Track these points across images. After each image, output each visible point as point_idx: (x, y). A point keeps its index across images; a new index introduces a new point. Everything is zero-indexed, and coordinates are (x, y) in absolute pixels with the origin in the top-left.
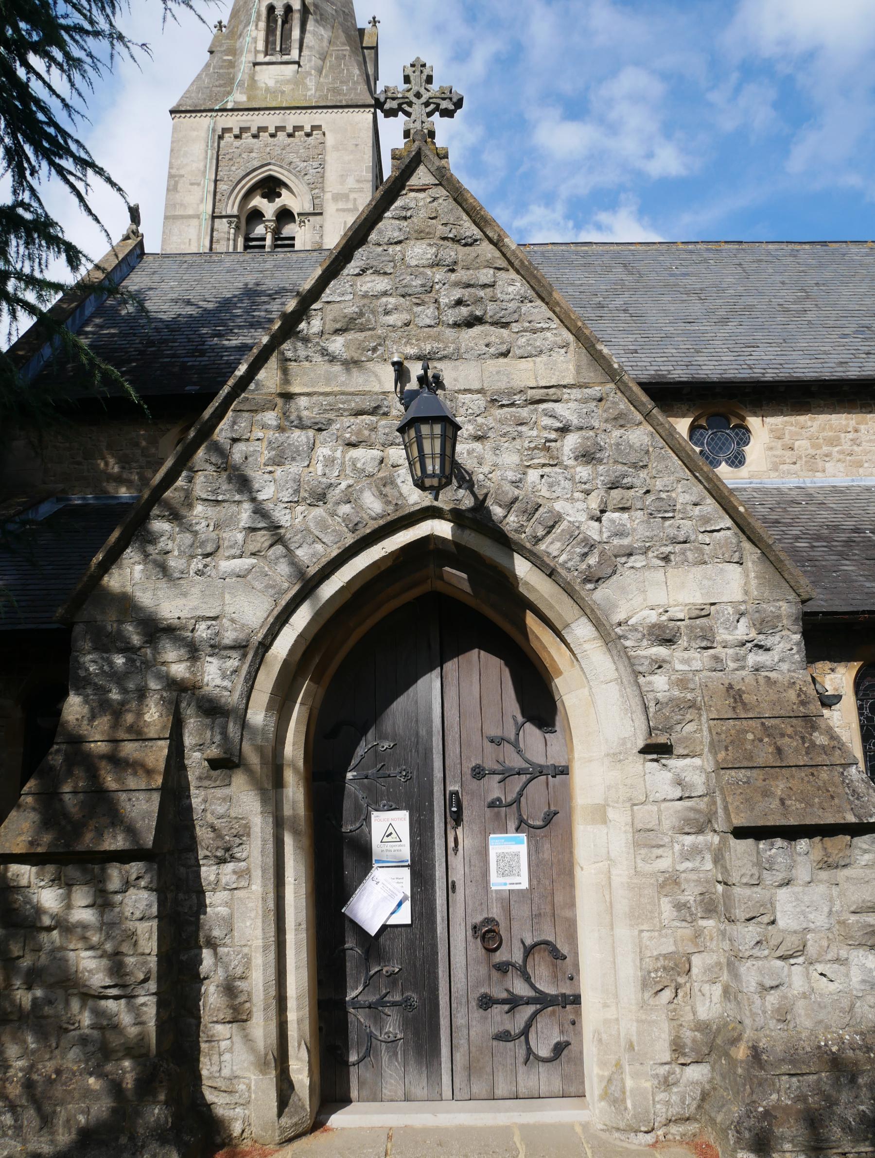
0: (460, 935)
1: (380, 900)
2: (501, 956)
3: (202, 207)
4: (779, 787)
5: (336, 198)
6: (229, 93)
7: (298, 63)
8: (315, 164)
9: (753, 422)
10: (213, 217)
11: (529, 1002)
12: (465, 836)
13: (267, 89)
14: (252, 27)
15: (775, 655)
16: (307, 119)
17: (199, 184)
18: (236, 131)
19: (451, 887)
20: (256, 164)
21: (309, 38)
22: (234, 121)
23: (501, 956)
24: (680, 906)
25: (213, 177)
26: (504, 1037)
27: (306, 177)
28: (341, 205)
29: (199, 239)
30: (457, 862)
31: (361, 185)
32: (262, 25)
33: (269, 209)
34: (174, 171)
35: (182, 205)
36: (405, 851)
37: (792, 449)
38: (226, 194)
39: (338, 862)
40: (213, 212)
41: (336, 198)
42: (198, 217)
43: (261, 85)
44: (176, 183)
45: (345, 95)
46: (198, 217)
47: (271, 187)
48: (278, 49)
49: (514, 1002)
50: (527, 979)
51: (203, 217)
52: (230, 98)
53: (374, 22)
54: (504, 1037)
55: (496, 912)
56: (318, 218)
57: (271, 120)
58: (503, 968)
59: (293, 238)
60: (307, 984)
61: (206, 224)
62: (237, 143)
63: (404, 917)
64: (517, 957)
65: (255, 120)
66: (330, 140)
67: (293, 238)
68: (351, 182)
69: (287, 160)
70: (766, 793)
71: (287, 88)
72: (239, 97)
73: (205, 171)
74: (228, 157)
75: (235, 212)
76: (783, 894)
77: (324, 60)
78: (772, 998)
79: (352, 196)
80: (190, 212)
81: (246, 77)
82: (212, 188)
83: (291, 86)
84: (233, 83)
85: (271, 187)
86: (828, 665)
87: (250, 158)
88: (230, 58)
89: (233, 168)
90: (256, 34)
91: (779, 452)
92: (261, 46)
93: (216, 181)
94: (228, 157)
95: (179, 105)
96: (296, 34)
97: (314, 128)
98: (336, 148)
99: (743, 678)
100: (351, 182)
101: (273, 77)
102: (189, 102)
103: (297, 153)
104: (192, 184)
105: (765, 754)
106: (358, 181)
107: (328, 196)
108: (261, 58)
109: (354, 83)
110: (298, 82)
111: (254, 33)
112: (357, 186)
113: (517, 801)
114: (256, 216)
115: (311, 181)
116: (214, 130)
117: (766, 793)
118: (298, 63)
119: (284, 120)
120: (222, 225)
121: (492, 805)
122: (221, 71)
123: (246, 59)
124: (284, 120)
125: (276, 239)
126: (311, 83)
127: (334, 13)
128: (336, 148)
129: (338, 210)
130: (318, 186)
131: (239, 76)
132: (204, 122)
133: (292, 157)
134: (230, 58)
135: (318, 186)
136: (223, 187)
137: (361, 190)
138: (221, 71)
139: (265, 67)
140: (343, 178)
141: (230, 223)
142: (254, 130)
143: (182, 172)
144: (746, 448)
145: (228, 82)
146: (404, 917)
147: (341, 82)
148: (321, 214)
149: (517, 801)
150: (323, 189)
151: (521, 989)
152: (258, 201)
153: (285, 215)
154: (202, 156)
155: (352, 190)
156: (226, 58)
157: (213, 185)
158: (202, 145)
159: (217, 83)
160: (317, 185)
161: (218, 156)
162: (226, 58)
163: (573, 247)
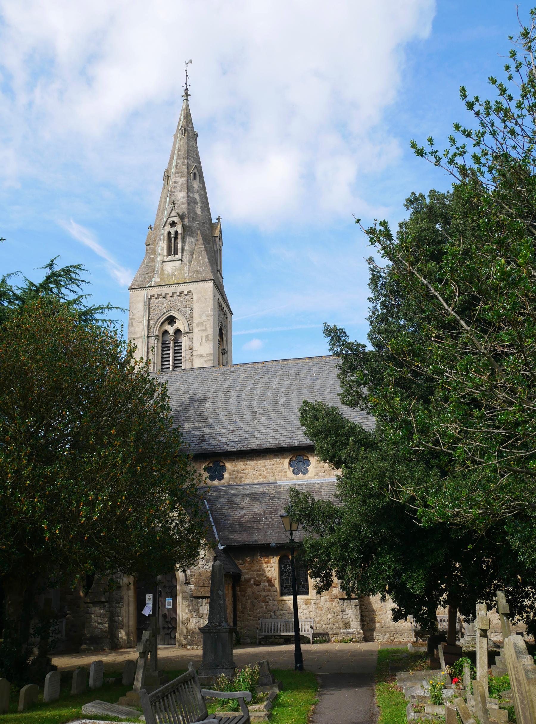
0: (160, 616)
1: (147, 611)
2: (167, 620)
3: (143, 333)
4: (202, 590)
5: (199, 324)
6: (153, 277)
7: (181, 260)
8: (189, 309)
9: (311, 459)
10: (148, 337)
11: (171, 628)
12: (161, 599)
13: (169, 274)
14: (161, 242)
15: (209, 566)
16: (184, 288)
17: (141, 322)
18: (156, 296)
19: (159, 608)
20: (165, 310)
21: (187, 247)
22: (154, 292)
23: (167, 620)
24: (189, 610)
25: (147, 319)
26: (166, 634)
27: (186, 315)
28: (200, 328)
29: (142, 348)
30: (160, 604)
31: (208, 318)
32: (166, 242)
33: (171, 329)
34: (131, 317)
35: (135, 332)
36: (152, 602)
37: (323, 467)
38: (153, 325)
39: (141, 604)
40: (148, 334)
41: (199, 324)
42: (141, 337)
43: (166, 272)
44: (132, 322)
45: (201, 274)
46: (141, 337)
47: (171, 320)
48: (173, 253)
49: (169, 628)
50: (171, 624)
51: (144, 337)
52: (153, 280)
53: (219, 219)
54: (166, 634)
55: (166, 612)
56: (191, 334)
57: (170, 290)
58: (167, 622)
59: (181, 342)
60: (211, 313)
61: (145, 340)
62: (157, 301)
63: (151, 613)
64: (170, 620)
65: (164, 290)
66: (195, 297)
67: (181, 342)
68: (204, 317)
69: (178, 308)
70: (200, 591)
71: (176, 273)
72: (156, 279)
73: (144, 316)
74: (153, 308)
75: (157, 334)
76: (201, 607)
77: (192, 255)
78: (197, 624)
79: (205, 323)
80: (139, 336)
81: (160, 268)
82: (147, 324)
83: (178, 272)
84: (154, 271)
85: (171, 320)
86: (272, 557)
87: (162, 308)
88: (153, 256)
89: (156, 313)
90: (163, 245)
91: (319, 469)
92: (165, 252)
93: (149, 320)
94: (153, 308)
95: (132, 285)
96: (180, 246)
97: (188, 292)
98: (198, 301)
99: (202, 570)
100: (204, 317)
101: (171, 267)
102: (136, 283)
103: (181, 304)
104: (139, 322)
105: (201, 585)
106: (207, 316)
107: (195, 324)
108: (166, 259)
109: (206, 267)
110: (181, 270)
111: (162, 245)
112: (206, 319)
113: (171, 592)
114: (166, 332)
115: (188, 317)
116: (147, 296)
117: (200, 591)
118: (181, 260)
119: (176, 289)
120: (152, 340)
121: (167, 593)
122: (149, 264)
123: (159, 259)
124: (176, 289)
125: (175, 343)
126: (186, 269)
127: (198, 226)
128: (198, 301)
129: (199, 331)
130: (191, 319)
131: (157, 268)
132: (142, 293)
133: (180, 306)
134: (153, 256)
135: (191, 319)
136: (152, 322)
137: (208, 320)
138: (149, 264)
139: (167, 263)
140: (201, 315)
141: (155, 339)
142: (163, 295)
143: (134, 317)
144: (308, 468)
145: (151, 270)
146: (151, 613)
147: (200, 267)
148: (192, 332)
149: (171, 592)
150: (192, 320)
151: (170, 626)
152: (168, 327)
153: (178, 332)
154: (142, 309)
155: (204, 321)
156: (151, 256)
157: (147, 322)
158: (142, 304)
159: (148, 272)
160: (189, 320)
161: (149, 307)
162: (151, 256)
163: (281, 362)
